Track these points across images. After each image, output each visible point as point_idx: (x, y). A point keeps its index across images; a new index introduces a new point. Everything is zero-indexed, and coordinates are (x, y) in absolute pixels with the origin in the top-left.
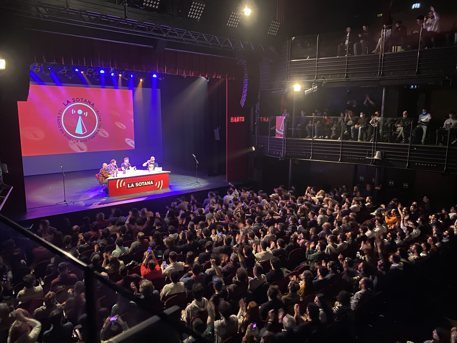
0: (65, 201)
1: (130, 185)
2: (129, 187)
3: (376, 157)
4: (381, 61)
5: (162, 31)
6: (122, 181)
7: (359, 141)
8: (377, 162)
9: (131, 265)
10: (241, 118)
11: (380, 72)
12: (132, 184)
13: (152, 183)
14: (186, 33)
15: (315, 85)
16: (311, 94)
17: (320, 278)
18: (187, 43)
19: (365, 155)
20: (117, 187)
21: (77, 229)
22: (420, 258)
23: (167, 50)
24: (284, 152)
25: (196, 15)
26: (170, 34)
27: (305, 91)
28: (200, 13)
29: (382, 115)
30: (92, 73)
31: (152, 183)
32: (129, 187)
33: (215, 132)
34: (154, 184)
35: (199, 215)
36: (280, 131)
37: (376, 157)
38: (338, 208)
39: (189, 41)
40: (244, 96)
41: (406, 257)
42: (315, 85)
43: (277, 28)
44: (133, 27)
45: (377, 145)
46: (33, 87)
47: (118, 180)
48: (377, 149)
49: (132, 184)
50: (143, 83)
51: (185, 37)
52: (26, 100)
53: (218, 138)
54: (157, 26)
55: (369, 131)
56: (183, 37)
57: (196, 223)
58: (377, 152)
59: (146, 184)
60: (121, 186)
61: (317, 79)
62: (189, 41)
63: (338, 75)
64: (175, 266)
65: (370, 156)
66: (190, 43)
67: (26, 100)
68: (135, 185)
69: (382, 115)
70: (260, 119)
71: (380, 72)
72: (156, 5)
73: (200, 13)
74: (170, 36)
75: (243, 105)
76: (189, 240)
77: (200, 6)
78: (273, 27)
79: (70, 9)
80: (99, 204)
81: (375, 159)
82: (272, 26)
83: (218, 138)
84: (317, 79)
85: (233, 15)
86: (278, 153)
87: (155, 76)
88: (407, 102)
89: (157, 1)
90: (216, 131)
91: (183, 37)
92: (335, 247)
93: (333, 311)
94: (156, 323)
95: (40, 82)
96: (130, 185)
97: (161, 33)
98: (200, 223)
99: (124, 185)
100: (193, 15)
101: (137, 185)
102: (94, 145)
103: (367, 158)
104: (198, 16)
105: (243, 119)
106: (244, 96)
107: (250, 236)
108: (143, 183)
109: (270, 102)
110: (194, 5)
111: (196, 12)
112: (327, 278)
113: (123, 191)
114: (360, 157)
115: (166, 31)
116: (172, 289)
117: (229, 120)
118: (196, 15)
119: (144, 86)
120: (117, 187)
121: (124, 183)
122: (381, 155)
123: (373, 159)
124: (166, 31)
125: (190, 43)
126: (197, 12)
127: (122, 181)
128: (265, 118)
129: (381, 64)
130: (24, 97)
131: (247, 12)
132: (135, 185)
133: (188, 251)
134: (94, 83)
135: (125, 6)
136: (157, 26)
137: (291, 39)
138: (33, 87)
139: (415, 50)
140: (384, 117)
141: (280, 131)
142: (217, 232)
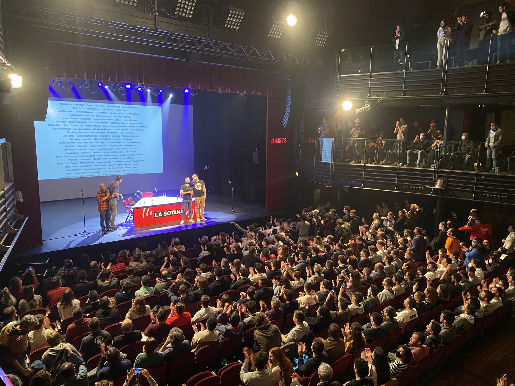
0: (85, 232)
1: (158, 214)
2: (156, 216)
3: (437, 186)
4: (444, 77)
5: (196, 42)
6: (149, 209)
7: (417, 168)
8: (439, 192)
10: (283, 139)
11: (443, 90)
12: (160, 213)
14: (223, 45)
15: (367, 103)
16: (362, 115)
17: (374, 327)
18: (224, 56)
19: (425, 183)
20: (144, 217)
21: (70, 292)
22: (490, 306)
23: (201, 64)
24: (332, 179)
25: (234, 25)
26: (205, 46)
27: (357, 110)
28: (238, 22)
29: (445, 138)
30: (118, 88)
32: (156, 216)
33: (253, 154)
34: (154, 214)
35: (235, 252)
36: (327, 157)
38: (391, 243)
39: (226, 54)
40: (287, 115)
42: (367, 103)
43: (324, 41)
44: (163, 38)
45: (439, 172)
46: (53, 108)
47: (145, 209)
48: (439, 177)
49: (160, 213)
50: (172, 99)
51: (221, 49)
52: (44, 120)
54: (191, 37)
55: (430, 154)
56: (219, 49)
57: (231, 261)
58: (439, 181)
59: (175, 213)
60: (147, 215)
61: (370, 96)
62: (226, 54)
63: (395, 93)
64: (206, 311)
65: (430, 184)
66: (227, 56)
67: (44, 120)
68: (163, 214)
70: (305, 140)
71: (443, 90)
72: (189, 14)
73: (238, 22)
74: (205, 49)
75: (285, 125)
76: (218, 277)
77: (238, 15)
78: (321, 37)
79: (93, 19)
80: (124, 236)
81: (437, 189)
82: (319, 37)
84: (370, 96)
85: (274, 27)
86: (324, 180)
87: (187, 91)
89: (193, 2)
90: (255, 154)
91: (219, 49)
92: (392, 292)
96: (158, 214)
97: (195, 45)
98: (235, 261)
99: (151, 214)
100: (231, 25)
101: (166, 214)
102: (108, 152)
103: (427, 187)
104: (237, 26)
106: (287, 115)
107: (295, 276)
108: (172, 211)
109: (309, 125)
110: (232, 14)
111: (234, 20)
112: (382, 327)
113: (152, 221)
114: (418, 186)
115: (200, 43)
116: (206, 337)
118: (234, 25)
119: (173, 102)
120: (144, 217)
121: (151, 212)
123: (434, 189)
124: (200, 43)
125: (227, 56)
126: (235, 22)
127: (149, 209)
128: (310, 140)
129: (444, 80)
130: (42, 116)
131: (292, 21)
132: (163, 214)
134: (121, 99)
135: (155, 15)
136: (191, 37)
137: (341, 51)
138: (53, 108)
139: (485, 65)
140: (447, 139)
141: (327, 157)
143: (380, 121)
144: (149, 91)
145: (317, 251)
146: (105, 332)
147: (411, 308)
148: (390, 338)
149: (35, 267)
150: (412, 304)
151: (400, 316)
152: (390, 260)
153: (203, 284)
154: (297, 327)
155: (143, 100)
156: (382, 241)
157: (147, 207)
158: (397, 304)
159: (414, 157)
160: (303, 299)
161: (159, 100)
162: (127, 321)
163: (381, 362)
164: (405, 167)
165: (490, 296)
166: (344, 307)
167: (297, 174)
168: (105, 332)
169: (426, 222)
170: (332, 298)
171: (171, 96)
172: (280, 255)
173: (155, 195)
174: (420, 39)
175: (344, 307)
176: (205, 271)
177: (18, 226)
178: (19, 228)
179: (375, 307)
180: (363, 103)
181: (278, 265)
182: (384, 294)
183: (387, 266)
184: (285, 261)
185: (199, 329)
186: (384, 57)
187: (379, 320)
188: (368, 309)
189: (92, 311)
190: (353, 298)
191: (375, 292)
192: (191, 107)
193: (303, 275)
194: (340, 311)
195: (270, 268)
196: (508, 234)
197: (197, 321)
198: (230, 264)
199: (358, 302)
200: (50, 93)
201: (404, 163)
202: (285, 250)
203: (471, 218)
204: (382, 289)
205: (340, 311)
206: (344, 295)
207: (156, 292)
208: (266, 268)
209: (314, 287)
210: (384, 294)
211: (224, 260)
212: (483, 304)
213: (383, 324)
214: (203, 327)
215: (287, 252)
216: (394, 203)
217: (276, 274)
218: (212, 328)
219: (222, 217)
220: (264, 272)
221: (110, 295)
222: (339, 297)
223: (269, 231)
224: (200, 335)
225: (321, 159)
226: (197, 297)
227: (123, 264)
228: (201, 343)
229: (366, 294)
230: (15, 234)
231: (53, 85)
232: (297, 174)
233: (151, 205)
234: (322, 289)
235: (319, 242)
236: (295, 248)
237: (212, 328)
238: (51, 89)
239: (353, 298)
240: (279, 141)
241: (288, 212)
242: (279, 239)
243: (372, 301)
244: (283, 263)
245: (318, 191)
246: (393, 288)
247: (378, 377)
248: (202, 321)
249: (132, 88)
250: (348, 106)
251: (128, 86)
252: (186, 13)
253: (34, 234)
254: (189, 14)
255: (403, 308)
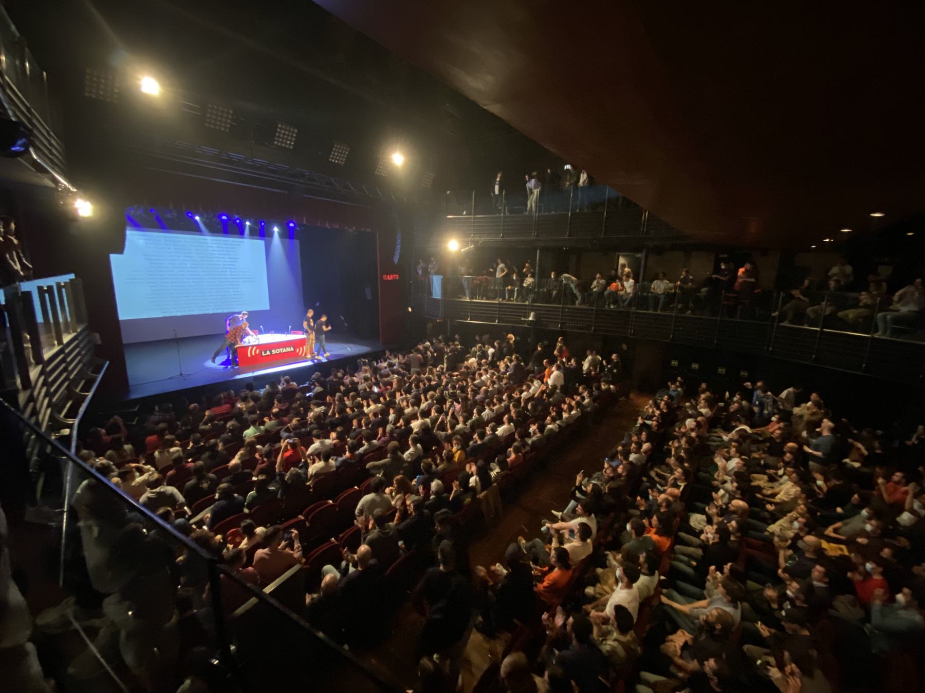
3: (531, 318)
9: (897, 291)
13: (292, 349)
16: (467, 253)
31: (292, 349)
34: (295, 350)
36: (437, 293)
37: (531, 318)
41: (560, 417)
46: (133, 236)
48: (532, 310)
53: (369, 297)
59: (284, 350)
65: (525, 317)
69: (537, 276)
83: (369, 297)
87: (292, 225)
88: (561, 259)
92: (492, 410)
93: (490, 476)
94: (255, 605)
95: (137, 226)
98: (351, 394)
101: (274, 352)
105: (397, 277)
111: (339, 155)
116: (322, 469)
117: (382, 277)
122: (535, 316)
130: (120, 250)
133: (777, 571)
134: (213, 230)
138: (133, 236)
141: (437, 293)
142: (371, 403)
143: (482, 261)
144: (248, 223)
145: (429, 380)
146: (211, 475)
147: (509, 423)
148: (496, 449)
149: (121, 416)
150: (510, 420)
151: (500, 431)
152: (493, 383)
153: (318, 418)
154: (411, 450)
155: (241, 232)
156: (484, 370)
157: (253, 346)
158: (498, 420)
159: (511, 292)
160: (415, 425)
161: (262, 233)
162: (235, 461)
163: (483, 473)
164: (504, 302)
165: (571, 408)
166: (453, 427)
167: (410, 310)
168: (211, 475)
169: (523, 350)
170: (443, 421)
171: (276, 229)
172: (395, 386)
173: (261, 332)
174: (515, 189)
175: (453, 427)
176: (318, 405)
177: (97, 371)
178: (99, 373)
179: (480, 425)
180: (466, 244)
181: (393, 395)
182: (486, 413)
183: (491, 389)
184: (400, 391)
185: (314, 462)
186: (485, 203)
187: (482, 435)
188: (473, 428)
189: (196, 454)
190: (461, 419)
191: (479, 413)
192: (297, 242)
193: (417, 402)
194: (450, 431)
195: (385, 399)
196: (586, 357)
197: (311, 454)
198: (346, 398)
199: (465, 422)
200: (128, 222)
201: (504, 298)
202: (399, 381)
203: (559, 344)
204: (484, 410)
205: (450, 431)
206: (453, 415)
207: (267, 431)
208: (382, 399)
209: (426, 414)
210: (486, 413)
211: (338, 394)
212: (565, 415)
213: (486, 438)
214: (317, 460)
215: (401, 382)
216: (495, 335)
217: (391, 404)
218: (326, 459)
219: (348, 349)
220: (380, 402)
221: (216, 437)
222: (449, 418)
223: (385, 364)
224: (315, 467)
225: (431, 294)
226: (309, 434)
227: (228, 405)
228: (317, 475)
229: (472, 414)
230: (94, 380)
231: (132, 213)
232: (410, 310)
233: (256, 343)
234: (433, 414)
235: (431, 372)
236: (409, 378)
237: (326, 459)
238: (130, 218)
239: (461, 419)
240: (390, 278)
241: (403, 345)
242: (394, 372)
243: (477, 420)
244: (398, 394)
245: (430, 325)
246: (495, 408)
247: (482, 486)
248: (318, 455)
249: (229, 219)
250: (454, 246)
251: (224, 218)
252: (286, 143)
253: (118, 378)
254: (290, 144)
255: (503, 423)
